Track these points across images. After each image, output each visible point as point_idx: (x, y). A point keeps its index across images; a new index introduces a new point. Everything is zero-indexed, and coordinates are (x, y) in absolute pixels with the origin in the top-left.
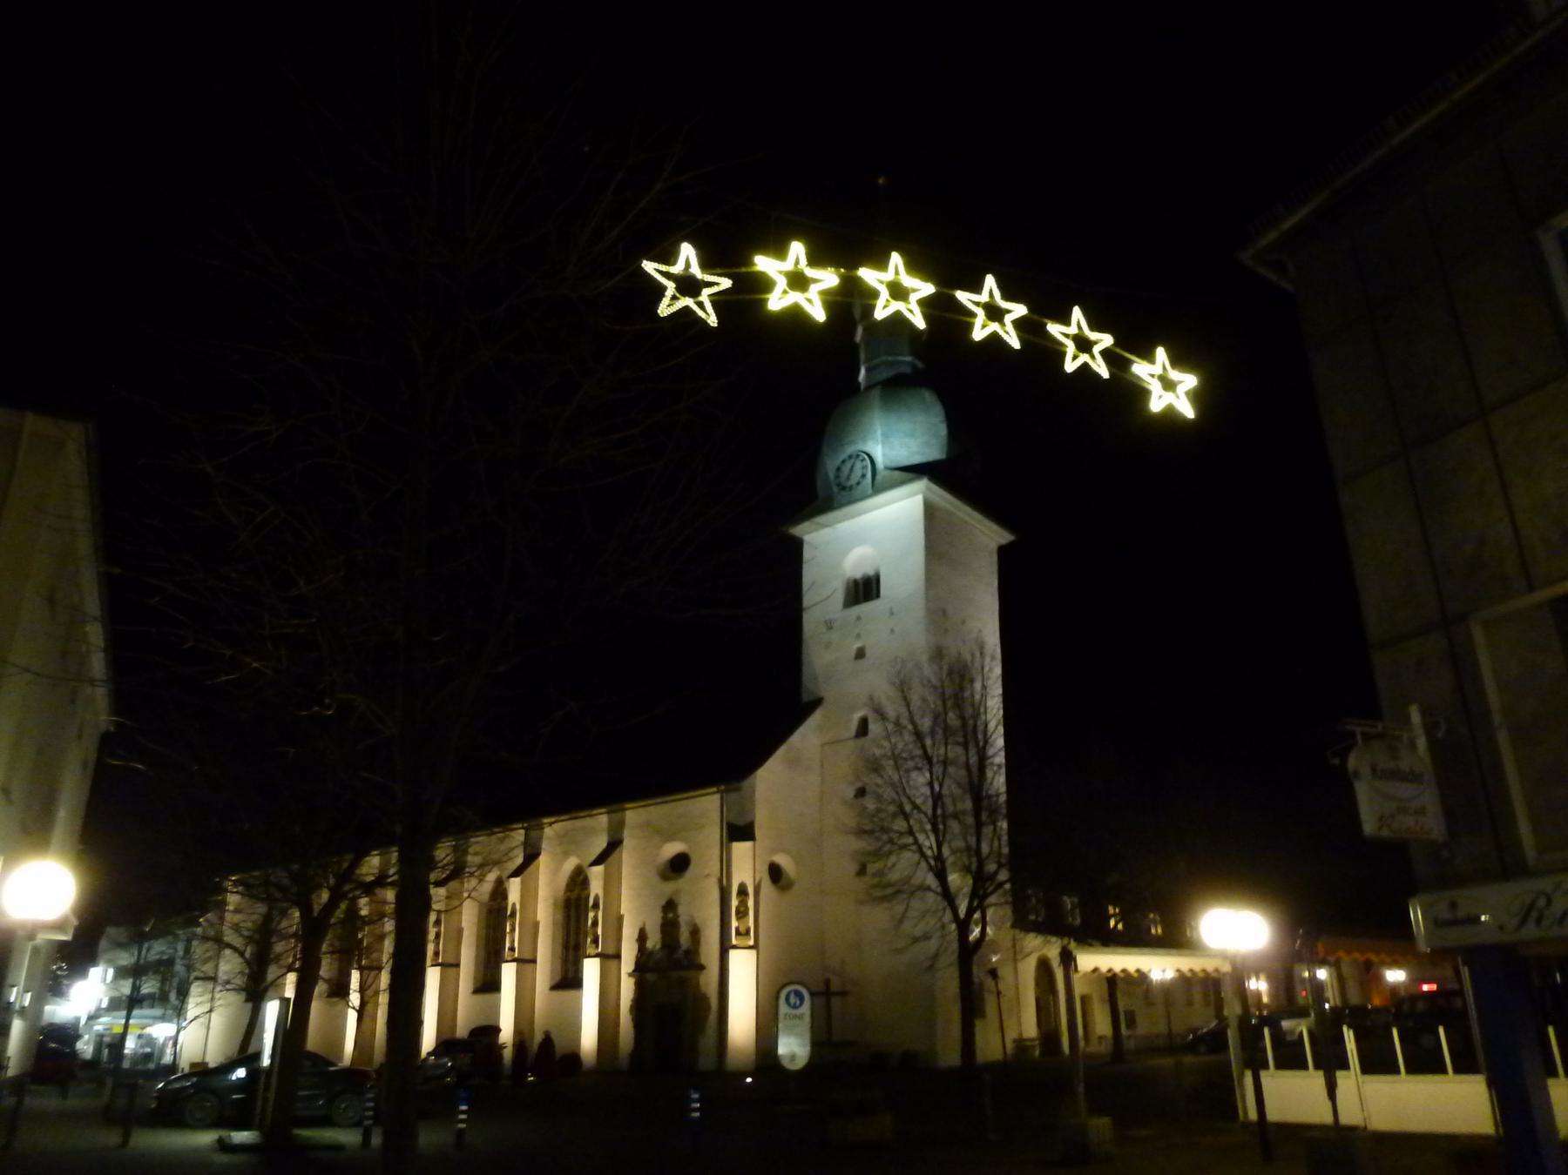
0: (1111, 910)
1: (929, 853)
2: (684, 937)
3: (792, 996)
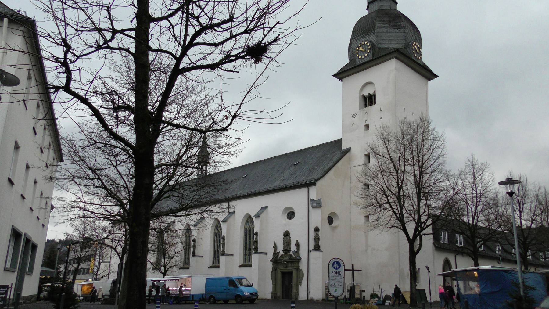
0: (530, 258)
1: (397, 212)
2: (293, 248)
3: (335, 264)
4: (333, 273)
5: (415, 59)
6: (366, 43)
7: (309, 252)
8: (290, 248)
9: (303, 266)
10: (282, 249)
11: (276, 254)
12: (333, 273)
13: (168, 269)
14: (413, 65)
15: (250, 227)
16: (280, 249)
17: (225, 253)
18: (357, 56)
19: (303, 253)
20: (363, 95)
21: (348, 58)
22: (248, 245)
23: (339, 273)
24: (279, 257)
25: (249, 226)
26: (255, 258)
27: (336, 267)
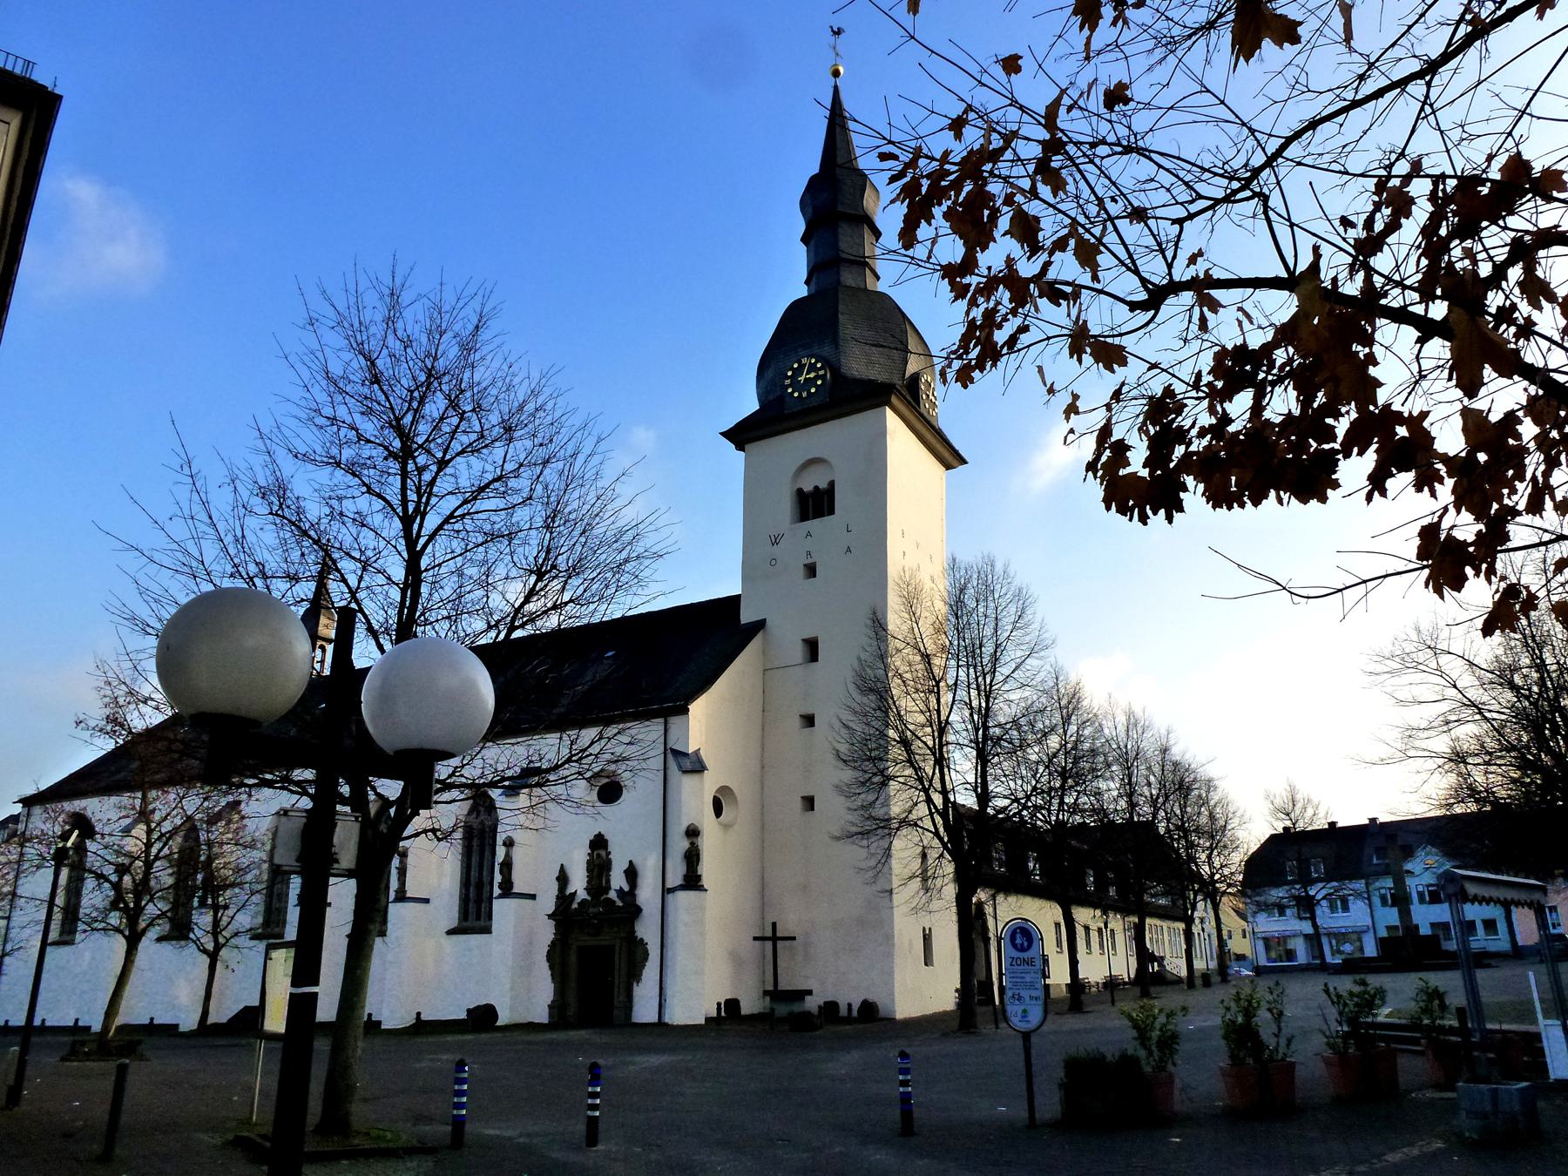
2: (618, 880)
3: (1018, 936)
5: (926, 414)
6: (813, 361)
7: (666, 891)
8: (608, 881)
9: (647, 929)
10: (585, 885)
11: (564, 899)
13: (227, 941)
14: (919, 426)
15: (482, 822)
16: (578, 884)
17: (408, 895)
18: (790, 390)
19: (647, 894)
20: (800, 492)
21: (756, 395)
22: (474, 874)
24: (575, 906)
26: (503, 910)
27: (1022, 945)
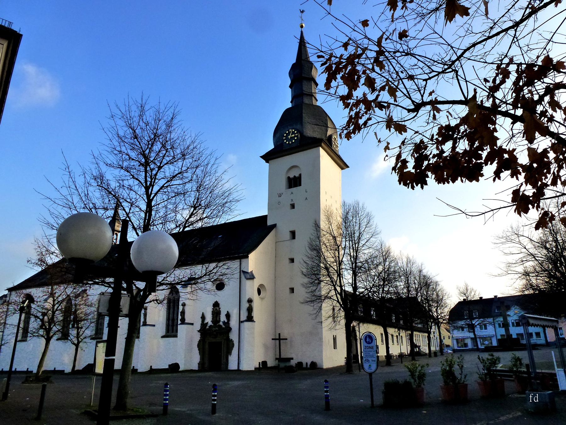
2: (223, 318)
3: (368, 338)
4: (366, 348)
5: (334, 150)
6: (293, 130)
7: (241, 322)
8: (220, 319)
9: (233, 336)
10: (211, 320)
11: (204, 325)
12: (366, 348)
14: (332, 154)
15: (174, 297)
16: (209, 319)
18: (285, 141)
19: (234, 323)
20: (289, 178)
21: (273, 143)
23: (372, 348)
24: (207, 327)
25: (173, 296)
26: (182, 329)
27: (369, 341)
